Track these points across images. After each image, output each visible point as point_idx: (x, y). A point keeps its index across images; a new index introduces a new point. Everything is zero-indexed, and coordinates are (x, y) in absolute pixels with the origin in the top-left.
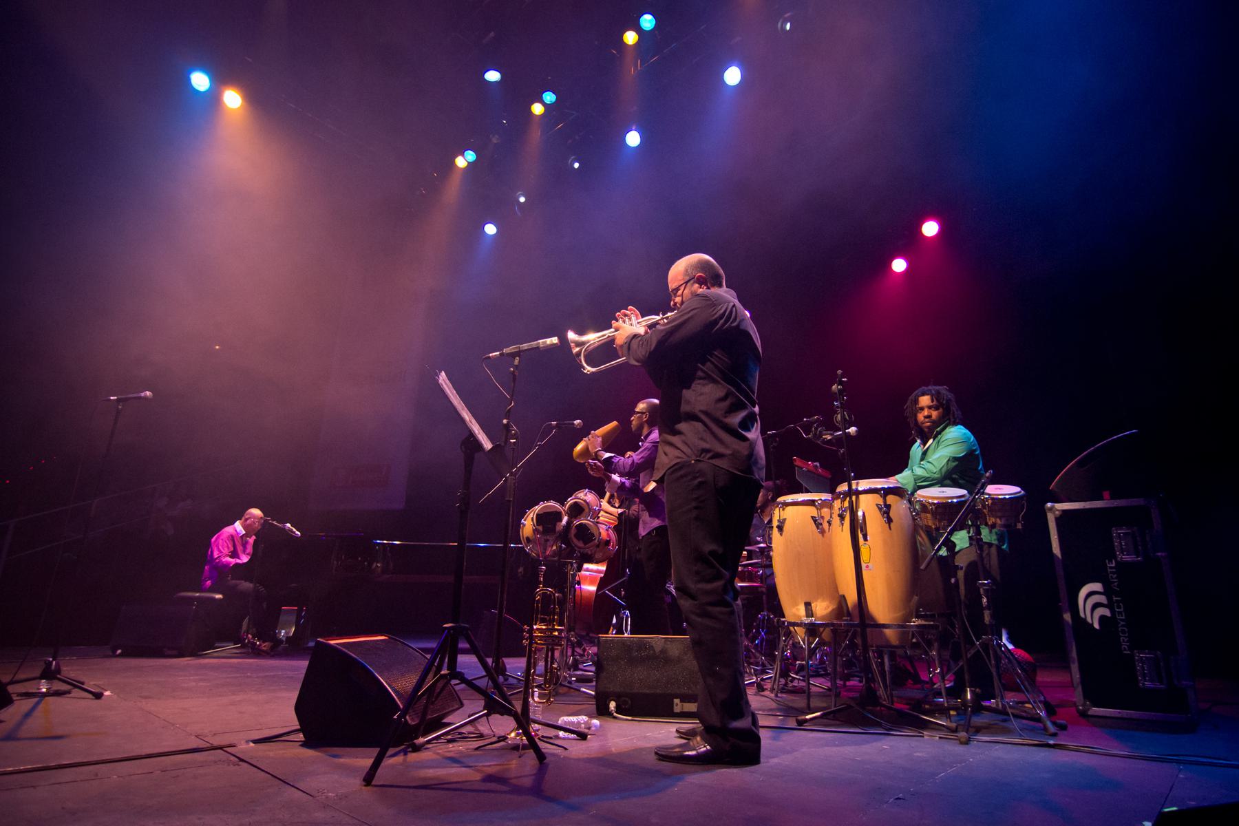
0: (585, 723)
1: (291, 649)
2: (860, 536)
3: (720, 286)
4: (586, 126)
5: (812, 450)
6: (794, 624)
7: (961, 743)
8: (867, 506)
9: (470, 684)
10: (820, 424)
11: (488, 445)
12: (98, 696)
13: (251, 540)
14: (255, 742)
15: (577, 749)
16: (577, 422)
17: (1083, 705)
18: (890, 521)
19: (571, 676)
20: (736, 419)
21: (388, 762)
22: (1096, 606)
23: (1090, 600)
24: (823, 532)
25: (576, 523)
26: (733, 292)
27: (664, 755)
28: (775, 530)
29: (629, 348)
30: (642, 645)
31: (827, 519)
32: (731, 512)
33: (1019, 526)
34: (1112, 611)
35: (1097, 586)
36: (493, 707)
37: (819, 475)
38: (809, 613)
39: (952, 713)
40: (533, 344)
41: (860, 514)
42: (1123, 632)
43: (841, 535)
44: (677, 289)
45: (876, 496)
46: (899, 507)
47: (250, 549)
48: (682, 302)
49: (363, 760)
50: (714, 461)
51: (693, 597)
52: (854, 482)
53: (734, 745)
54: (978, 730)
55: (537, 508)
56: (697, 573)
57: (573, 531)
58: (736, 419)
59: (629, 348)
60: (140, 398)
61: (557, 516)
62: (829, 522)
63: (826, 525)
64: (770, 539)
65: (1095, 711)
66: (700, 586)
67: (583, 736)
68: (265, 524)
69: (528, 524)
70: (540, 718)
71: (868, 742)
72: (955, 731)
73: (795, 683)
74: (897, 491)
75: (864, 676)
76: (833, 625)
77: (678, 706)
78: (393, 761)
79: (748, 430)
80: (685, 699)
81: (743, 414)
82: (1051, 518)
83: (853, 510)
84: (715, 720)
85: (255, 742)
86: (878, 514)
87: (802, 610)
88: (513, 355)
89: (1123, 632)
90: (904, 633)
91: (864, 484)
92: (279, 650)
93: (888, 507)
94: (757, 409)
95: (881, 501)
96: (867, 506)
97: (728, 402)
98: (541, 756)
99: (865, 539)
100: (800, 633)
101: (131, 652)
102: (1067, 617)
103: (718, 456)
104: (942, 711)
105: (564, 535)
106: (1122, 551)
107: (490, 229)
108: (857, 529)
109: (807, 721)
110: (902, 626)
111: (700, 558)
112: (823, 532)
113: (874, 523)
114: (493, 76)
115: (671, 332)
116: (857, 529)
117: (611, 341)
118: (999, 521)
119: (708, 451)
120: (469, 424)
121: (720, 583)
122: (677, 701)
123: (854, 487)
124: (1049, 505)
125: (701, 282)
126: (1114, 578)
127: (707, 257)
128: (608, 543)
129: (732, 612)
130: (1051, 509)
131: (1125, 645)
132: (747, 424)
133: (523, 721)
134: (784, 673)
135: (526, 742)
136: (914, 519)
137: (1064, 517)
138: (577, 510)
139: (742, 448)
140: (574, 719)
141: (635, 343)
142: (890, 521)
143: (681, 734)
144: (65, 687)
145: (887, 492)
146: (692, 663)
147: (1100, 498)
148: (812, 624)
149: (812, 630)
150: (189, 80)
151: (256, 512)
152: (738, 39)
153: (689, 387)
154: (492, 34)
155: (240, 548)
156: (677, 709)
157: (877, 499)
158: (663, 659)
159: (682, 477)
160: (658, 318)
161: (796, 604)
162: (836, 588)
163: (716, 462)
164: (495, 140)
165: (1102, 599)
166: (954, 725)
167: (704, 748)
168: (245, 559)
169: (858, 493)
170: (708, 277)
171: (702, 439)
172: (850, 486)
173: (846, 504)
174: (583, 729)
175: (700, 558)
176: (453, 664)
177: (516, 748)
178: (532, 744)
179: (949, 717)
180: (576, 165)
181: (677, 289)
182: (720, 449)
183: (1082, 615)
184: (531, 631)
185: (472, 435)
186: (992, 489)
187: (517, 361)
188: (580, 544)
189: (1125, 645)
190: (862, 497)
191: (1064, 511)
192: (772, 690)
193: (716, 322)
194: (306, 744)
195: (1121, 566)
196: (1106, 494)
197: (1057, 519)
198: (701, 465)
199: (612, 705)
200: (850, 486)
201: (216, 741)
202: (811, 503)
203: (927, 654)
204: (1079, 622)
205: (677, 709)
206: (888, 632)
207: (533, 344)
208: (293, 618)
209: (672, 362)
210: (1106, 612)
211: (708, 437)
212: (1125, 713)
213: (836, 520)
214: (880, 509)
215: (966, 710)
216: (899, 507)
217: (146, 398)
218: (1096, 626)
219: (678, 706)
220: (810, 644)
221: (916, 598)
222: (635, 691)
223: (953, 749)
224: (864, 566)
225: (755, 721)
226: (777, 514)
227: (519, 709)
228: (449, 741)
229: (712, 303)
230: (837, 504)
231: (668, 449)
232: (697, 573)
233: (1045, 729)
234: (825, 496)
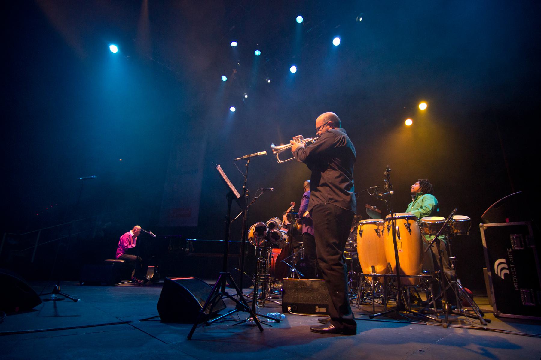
0: (279, 315)
1: (154, 283)
3: (339, 127)
4: (275, 63)
6: (367, 275)
7: (444, 328)
8: (400, 225)
9: (231, 297)
11: (238, 196)
12: (76, 301)
13: (136, 239)
14: (141, 320)
15: (276, 327)
16: (272, 189)
18: (410, 231)
19: (270, 296)
20: (343, 186)
21: (197, 330)
22: (502, 269)
23: (500, 266)
24: (380, 236)
26: (344, 130)
27: (314, 330)
29: (297, 154)
30: (302, 283)
31: (382, 230)
32: (342, 226)
33: (468, 234)
34: (510, 271)
35: (503, 260)
36: (240, 308)
37: (376, 212)
39: (438, 315)
40: (255, 154)
41: (397, 228)
42: (515, 280)
43: (388, 237)
44: (320, 128)
46: (414, 225)
47: (135, 242)
48: (322, 134)
49: (188, 328)
50: (334, 204)
51: (325, 262)
52: (394, 214)
53: (346, 327)
54: (451, 322)
55: (256, 225)
56: (328, 252)
57: (271, 235)
58: (343, 186)
59: (297, 154)
60: (92, 178)
61: (265, 228)
62: (383, 232)
63: (381, 233)
64: (356, 239)
65: (502, 315)
66: (329, 257)
67: (278, 321)
68: (141, 231)
69: (252, 231)
70: (259, 313)
71: (402, 326)
72: (441, 322)
73: (366, 301)
74: (413, 218)
75: (399, 297)
76: (385, 275)
77: (318, 309)
78: (200, 331)
79: (349, 190)
80: (321, 306)
81: (347, 183)
83: (394, 226)
84: (337, 315)
85: (141, 320)
86: (405, 228)
87: (370, 269)
88: (247, 159)
89: (515, 280)
91: (398, 215)
92: (146, 284)
93: (409, 225)
94: (353, 181)
95: (406, 222)
96: (400, 225)
97: (340, 179)
98: (261, 330)
99: (399, 238)
100: (370, 280)
101: (88, 284)
103: (336, 201)
104: (433, 313)
105: (267, 237)
106: (515, 245)
107: (233, 109)
108: (396, 234)
110: (416, 277)
111: (329, 245)
112: (380, 236)
113: (403, 232)
114: (234, 44)
116: (396, 234)
117: (290, 149)
118: (459, 231)
119: (332, 199)
121: (338, 256)
122: (317, 307)
124: (481, 224)
125: (330, 125)
126: (511, 257)
127: (333, 114)
128: (285, 240)
129: (343, 268)
130: (482, 226)
131: (516, 286)
132: (348, 188)
133: (253, 313)
134: (362, 297)
135: (255, 323)
136: (421, 230)
137: (488, 231)
138: (273, 226)
139: (348, 198)
140: (274, 314)
141: (300, 152)
142: (410, 231)
143: (320, 321)
144: (61, 297)
146: (326, 291)
147: (505, 222)
148: (375, 275)
149: (375, 278)
150: (109, 50)
151: (138, 227)
152: (294, 57)
153: (324, 172)
154: (234, 27)
155: (132, 241)
156: (317, 311)
158: (310, 289)
159: (320, 210)
160: (311, 139)
161: (368, 267)
162: (386, 260)
163: (336, 204)
164: (235, 72)
165: (506, 266)
166: (440, 320)
167: (332, 327)
168: (134, 246)
169: (396, 219)
170: (333, 123)
171: (329, 194)
172: (392, 216)
173: (391, 223)
175: (329, 245)
176: (223, 290)
177: (250, 325)
178: (258, 324)
179: (437, 316)
180: (269, 81)
181: (320, 128)
182: (337, 198)
183: (496, 273)
185: (231, 191)
186: (456, 217)
187: (248, 161)
188: (274, 240)
189: (516, 286)
190: (397, 220)
191: (488, 227)
192: (357, 304)
193: (336, 144)
194: (161, 322)
195: (514, 251)
197: (485, 231)
198: (328, 205)
199: (289, 308)
200: (392, 216)
201: (125, 320)
202: (374, 223)
204: (495, 277)
205: (317, 311)
206: (410, 279)
207: (255, 154)
208: (153, 271)
209: (317, 160)
211: (332, 193)
212: (516, 316)
213: (386, 231)
214: (406, 226)
215: (445, 313)
216: (414, 225)
217: (94, 178)
218: (503, 278)
219: (318, 309)
221: (422, 264)
222: (299, 302)
223: (440, 330)
224: (398, 250)
225: (353, 317)
226: (359, 228)
227: (251, 307)
228: (222, 322)
229: (336, 135)
230: (386, 224)
231: (314, 198)
232: (328, 252)
234: (382, 221)
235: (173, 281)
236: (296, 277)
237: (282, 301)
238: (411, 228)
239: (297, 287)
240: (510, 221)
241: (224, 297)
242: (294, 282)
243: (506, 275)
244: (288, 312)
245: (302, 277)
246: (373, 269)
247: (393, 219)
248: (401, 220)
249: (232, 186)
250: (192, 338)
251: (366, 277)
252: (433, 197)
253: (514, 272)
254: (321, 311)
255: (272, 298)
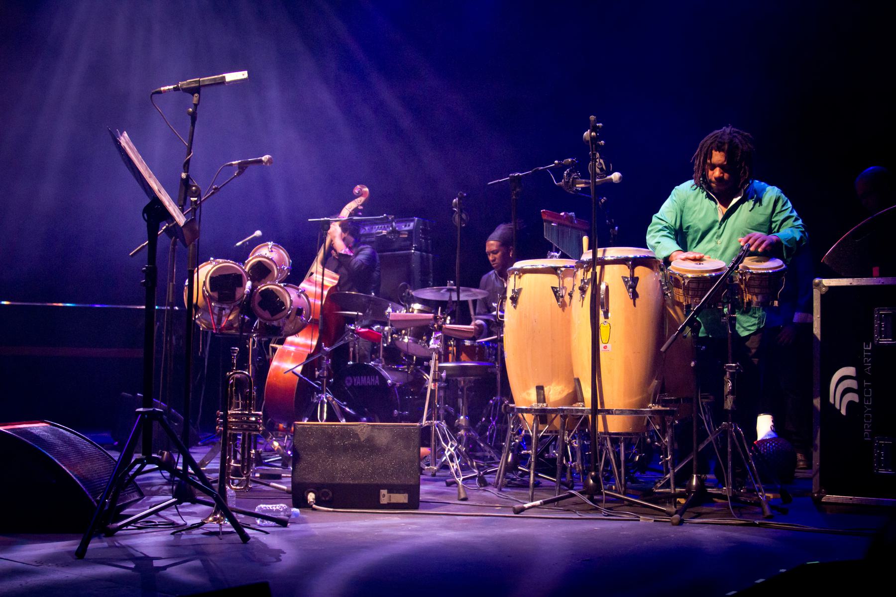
0: (285, 511)
2: (601, 312)
5: (562, 200)
8: (613, 278)
10: (574, 168)
17: (819, 492)
18: (635, 295)
22: (847, 391)
24: (563, 306)
25: (262, 287)
28: (508, 303)
30: (345, 433)
31: (569, 290)
34: (861, 398)
35: (850, 371)
38: (541, 398)
41: (603, 287)
43: (581, 309)
45: (623, 267)
61: (238, 280)
63: (567, 298)
67: (283, 523)
76: (635, 412)
77: (385, 497)
80: (392, 489)
82: (817, 295)
87: (533, 395)
90: (641, 419)
91: (612, 253)
93: (635, 280)
95: (627, 273)
96: (613, 278)
98: (245, 538)
99: (606, 317)
102: (817, 402)
105: (246, 307)
108: (599, 305)
109: (523, 509)
115: (402, 222)
116: (599, 305)
118: (755, 299)
120: (159, 194)
122: (384, 492)
123: (600, 255)
124: (817, 280)
130: (818, 285)
142: (635, 295)
145: (635, 262)
147: (869, 275)
149: (542, 416)
156: (384, 501)
157: (623, 270)
158: (370, 447)
161: (526, 388)
162: (572, 371)
165: (853, 384)
169: (604, 263)
173: (589, 276)
174: (282, 516)
183: (831, 401)
184: (225, 417)
185: (156, 202)
188: (267, 314)
189: (866, 432)
190: (607, 267)
191: (831, 288)
195: (878, 348)
196: (876, 270)
197: (823, 297)
199: (311, 497)
202: (554, 270)
203: (659, 440)
205: (384, 501)
210: (853, 397)
212: (855, 499)
213: (577, 294)
214: (626, 283)
218: (843, 412)
219: (385, 497)
220: (538, 432)
221: (655, 382)
222: (337, 481)
224: (602, 346)
226: (512, 284)
230: (580, 273)
233: (763, 513)
235: (354, 410)
236: (332, 417)
237: (293, 482)
238: (638, 289)
239: (333, 443)
240: (881, 276)
241: (148, 467)
242: (322, 429)
243: (850, 404)
244: (309, 506)
245: (349, 418)
246: (538, 394)
247: (596, 262)
248: (616, 267)
249: (163, 191)
250: (87, 556)
251: (520, 415)
252: (647, 237)
253: (868, 398)
254: (393, 501)
255: (261, 477)
